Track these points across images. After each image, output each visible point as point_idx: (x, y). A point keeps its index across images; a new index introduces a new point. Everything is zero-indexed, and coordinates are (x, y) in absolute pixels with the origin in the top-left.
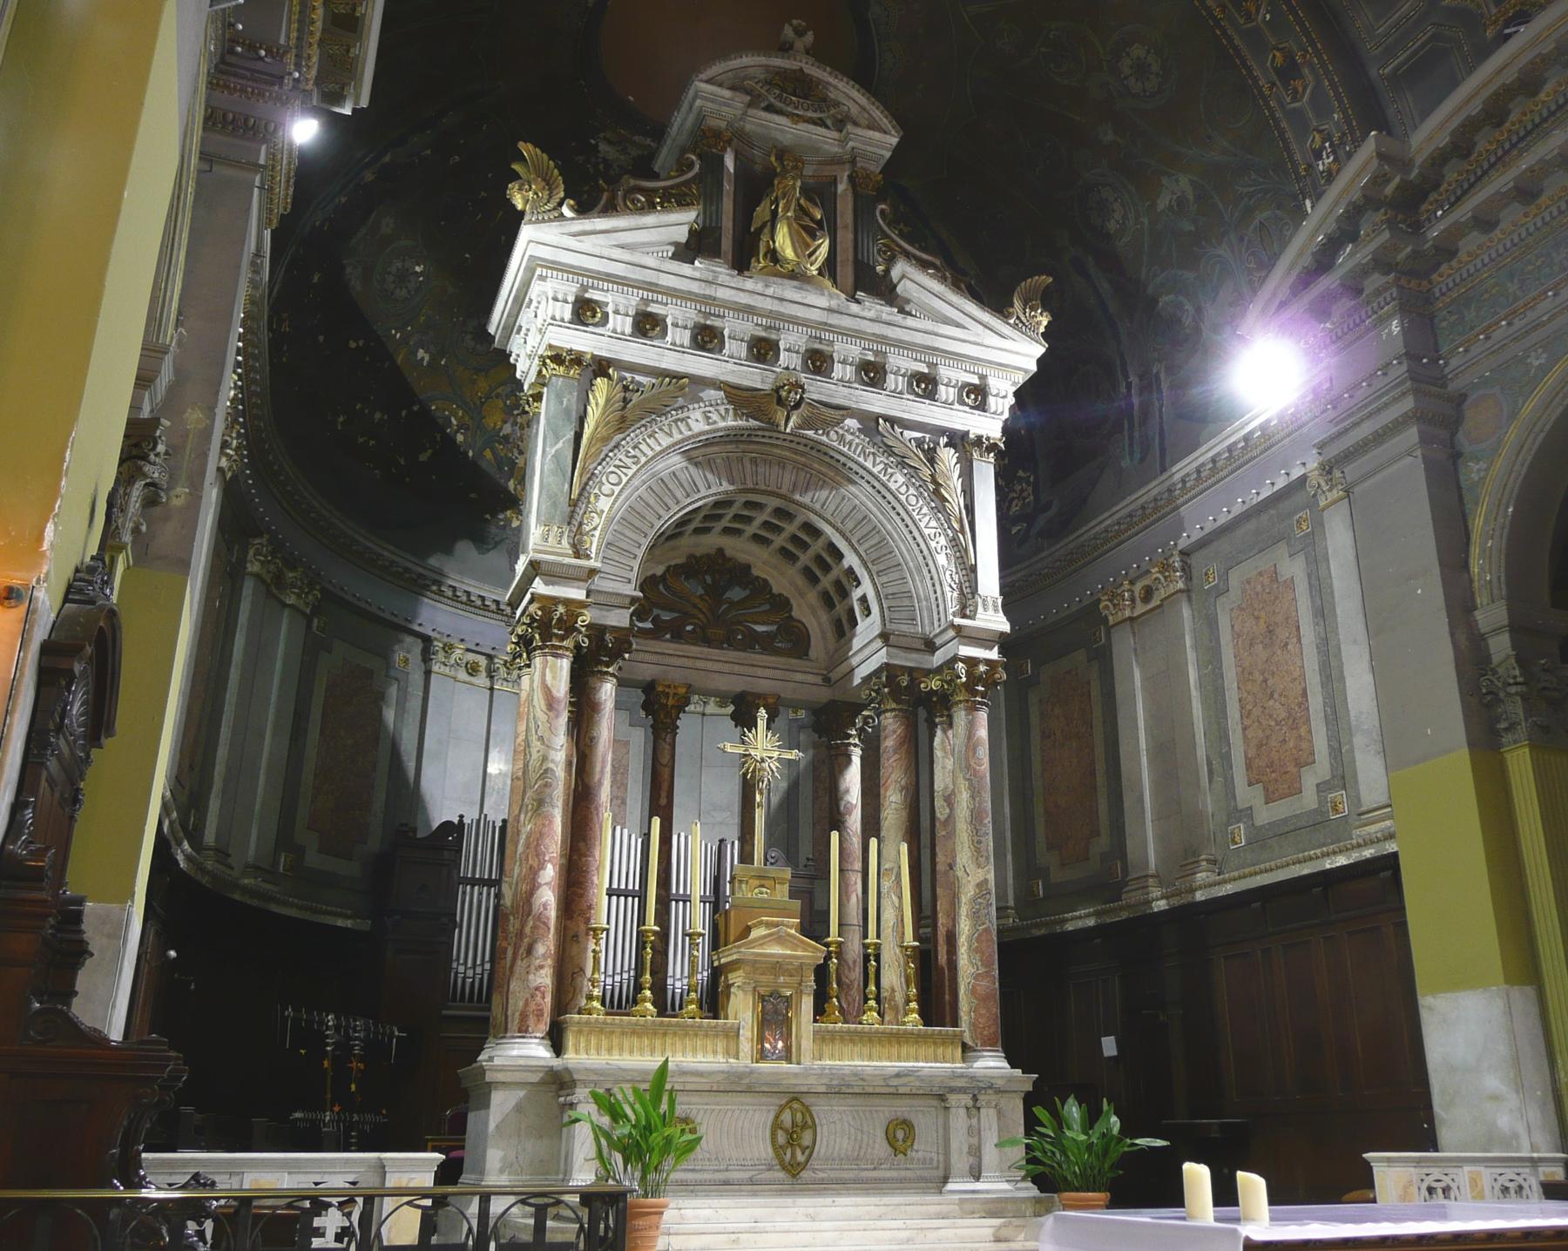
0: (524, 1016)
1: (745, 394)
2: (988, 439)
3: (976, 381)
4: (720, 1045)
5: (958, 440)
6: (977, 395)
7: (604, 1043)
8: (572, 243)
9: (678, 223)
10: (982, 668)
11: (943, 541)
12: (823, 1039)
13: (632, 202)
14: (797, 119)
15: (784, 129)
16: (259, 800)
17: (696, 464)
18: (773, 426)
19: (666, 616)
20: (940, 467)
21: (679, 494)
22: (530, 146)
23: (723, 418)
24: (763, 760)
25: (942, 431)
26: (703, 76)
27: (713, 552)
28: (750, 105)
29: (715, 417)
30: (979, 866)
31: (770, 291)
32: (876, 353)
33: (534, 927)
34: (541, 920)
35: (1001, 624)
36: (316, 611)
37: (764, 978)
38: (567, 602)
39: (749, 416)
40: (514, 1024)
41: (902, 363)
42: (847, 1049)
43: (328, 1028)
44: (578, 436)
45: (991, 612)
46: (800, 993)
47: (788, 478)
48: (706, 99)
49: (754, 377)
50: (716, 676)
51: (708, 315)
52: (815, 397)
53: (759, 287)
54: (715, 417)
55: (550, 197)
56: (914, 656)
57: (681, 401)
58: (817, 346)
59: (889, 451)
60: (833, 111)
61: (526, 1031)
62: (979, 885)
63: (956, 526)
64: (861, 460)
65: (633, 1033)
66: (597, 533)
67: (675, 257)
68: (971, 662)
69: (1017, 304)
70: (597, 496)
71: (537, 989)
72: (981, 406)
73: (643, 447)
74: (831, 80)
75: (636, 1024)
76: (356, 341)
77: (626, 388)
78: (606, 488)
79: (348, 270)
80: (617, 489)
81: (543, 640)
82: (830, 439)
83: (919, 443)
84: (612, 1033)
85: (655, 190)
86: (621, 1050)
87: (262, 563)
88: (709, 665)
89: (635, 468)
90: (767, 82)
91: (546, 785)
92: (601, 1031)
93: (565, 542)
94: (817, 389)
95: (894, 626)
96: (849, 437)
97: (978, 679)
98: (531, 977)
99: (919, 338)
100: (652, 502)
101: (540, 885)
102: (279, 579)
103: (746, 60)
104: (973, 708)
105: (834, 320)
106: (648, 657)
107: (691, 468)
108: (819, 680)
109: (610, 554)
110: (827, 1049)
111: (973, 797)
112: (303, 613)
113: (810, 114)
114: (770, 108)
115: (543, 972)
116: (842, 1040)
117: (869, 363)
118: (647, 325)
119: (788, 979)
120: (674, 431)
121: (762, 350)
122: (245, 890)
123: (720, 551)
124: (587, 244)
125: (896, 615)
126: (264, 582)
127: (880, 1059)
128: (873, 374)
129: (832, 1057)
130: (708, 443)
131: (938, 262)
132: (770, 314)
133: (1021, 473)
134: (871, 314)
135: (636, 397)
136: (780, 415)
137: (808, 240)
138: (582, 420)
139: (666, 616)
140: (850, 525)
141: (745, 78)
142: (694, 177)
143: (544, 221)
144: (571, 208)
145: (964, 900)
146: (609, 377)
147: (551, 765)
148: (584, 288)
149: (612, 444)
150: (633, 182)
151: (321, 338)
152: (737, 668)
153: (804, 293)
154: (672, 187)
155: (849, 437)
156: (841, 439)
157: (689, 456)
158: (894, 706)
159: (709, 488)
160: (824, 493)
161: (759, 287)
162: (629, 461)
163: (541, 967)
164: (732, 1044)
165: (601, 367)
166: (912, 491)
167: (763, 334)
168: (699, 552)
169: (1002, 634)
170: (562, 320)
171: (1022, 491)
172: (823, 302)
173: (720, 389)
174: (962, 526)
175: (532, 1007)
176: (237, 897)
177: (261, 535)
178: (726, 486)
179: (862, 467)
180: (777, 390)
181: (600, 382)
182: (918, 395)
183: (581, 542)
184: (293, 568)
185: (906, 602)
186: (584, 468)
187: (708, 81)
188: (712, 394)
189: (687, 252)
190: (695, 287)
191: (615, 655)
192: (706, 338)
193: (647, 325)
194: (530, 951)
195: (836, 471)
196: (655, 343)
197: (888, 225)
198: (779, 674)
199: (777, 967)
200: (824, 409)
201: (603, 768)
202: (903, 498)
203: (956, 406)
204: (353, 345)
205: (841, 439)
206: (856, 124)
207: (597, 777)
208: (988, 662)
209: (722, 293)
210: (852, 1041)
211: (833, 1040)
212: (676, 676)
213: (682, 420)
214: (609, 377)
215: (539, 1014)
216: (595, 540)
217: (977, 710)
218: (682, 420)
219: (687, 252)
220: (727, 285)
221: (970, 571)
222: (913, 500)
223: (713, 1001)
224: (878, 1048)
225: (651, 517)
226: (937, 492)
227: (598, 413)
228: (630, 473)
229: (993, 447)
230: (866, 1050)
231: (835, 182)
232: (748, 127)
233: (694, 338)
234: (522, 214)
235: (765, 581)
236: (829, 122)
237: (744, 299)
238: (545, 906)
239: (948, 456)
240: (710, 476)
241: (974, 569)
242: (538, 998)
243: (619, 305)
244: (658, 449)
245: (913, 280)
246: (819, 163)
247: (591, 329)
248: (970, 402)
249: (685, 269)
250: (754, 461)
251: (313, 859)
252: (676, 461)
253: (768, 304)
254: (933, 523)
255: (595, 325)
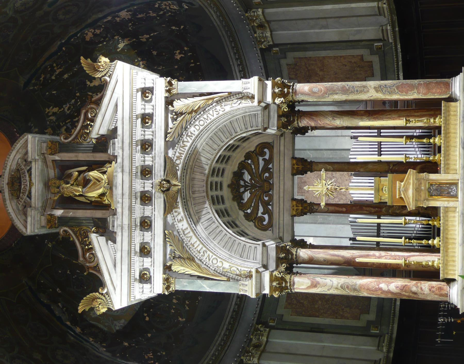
0: (441, 295)
1: (167, 205)
2: (166, 87)
3: (139, 94)
4: (451, 214)
5: (169, 102)
6: (146, 92)
7: (450, 268)
8: (118, 289)
9: (97, 241)
10: (277, 90)
11: (218, 108)
12: (448, 169)
13: (91, 258)
14: (31, 184)
15: (37, 189)
16: (351, 346)
17: (200, 219)
18: (178, 191)
19: (261, 210)
20: (184, 110)
21: (214, 226)
22: (79, 308)
23: (179, 213)
24: (327, 189)
25: (166, 109)
26: (24, 230)
27: (230, 190)
28: (31, 207)
29: (179, 217)
30: (368, 91)
31: (120, 200)
32: (137, 145)
33: (406, 292)
34: (404, 288)
35: (255, 80)
36: (266, 325)
37: (423, 196)
38: (271, 281)
39: (176, 202)
40: (444, 299)
41: (139, 133)
42: (452, 157)
43: (444, 321)
44: (199, 277)
45: (248, 85)
46: (428, 180)
47: (198, 176)
48: (34, 228)
49: (159, 201)
50: (285, 187)
51: (136, 225)
52: (162, 173)
53: (119, 205)
54: (179, 217)
55: (99, 298)
56: (272, 114)
57: (175, 233)
58: (139, 174)
59: (181, 135)
60: (23, 167)
61: (447, 294)
62: (377, 91)
63: (210, 102)
64: (187, 148)
65: (447, 251)
66: (239, 268)
67: (114, 242)
68: (274, 95)
69: (98, 75)
70: (223, 268)
71: (430, 290)
72: (151, 90)
73: (199, 249)
74: (8, 169)
75: (443, 251)
76: (145, 317)
77: (174, 257)
78: (219, 264)
79: (117, 328)
80: (219, 260)
81: (288, 289)
82: (180, 163)
83: (174, 120)
84: (447, 260)
85: (83, 249)
86: (454, 256)
87: (253, 357)
88: (282, 190)
89: (208, 252)
90: (18, 197)
91: (348, 287)
92: (446, 265)
93: (246, 283)
94: (159, 173)
95: (260, 125)
96: (177, 154)
97: (283, 91)
98: (425, 293)
99: (127, 127)
100: (220, 238)
101: (389, 290)
102: (257, 346)
103: (10, 210)
104: (295, 92)
105: (127, 169)
106: (281, 218)
107: (202, 220)
108: (282, 138)
109: (245, 256)
110: (452, 167)
111: (337, 94)
112: (269, 331)
113: (28, 178)
114: (29, 196)
115: (423, 288)
116: (448, 160)
117: (141, 147)
118: (145, 251)
119: (423, 185)
120: (189, 235)
121: (146, 198)
122: (388, 352)
123: (229, 186)
124: (117, 282)
125: (254, 124)
126: (260, 355)
127: (456, 142)
128: (146, 146)
129: (455, 165)
130: (190, 216)
131: (84, 111)
132: (130, 199)
133: (157, 6)
134: (120, 151)
135: (178, 253)
136: (174, 189)
137: (92, 183)
138: (191, 276)
139: (261, 210)
140: (215, 146)
141: (18, 209)
142: (71, 230)
143: (111, 301)
144: (103, 289)
145: (384, 97)
146: (171, 265)
147: (339, 285)
148: (135, 279)
149: (199, 262)
150: (81, 259)
151: (149, 335)
152: (282, 178)
153: (118, 185)
154: (79, 240)
155: (177, 154)
156: (179, 158)
157: (196, 223)
158: (296, 122)
159: (208, 212)
160: (203, 159)
161: (119, 205)
162: (206, 255)
163: (421, 288)
164: (451, 209)
165: (167, 268)
166: (197, 123)
167: (139, 199)
168: (231, 196)
169: (260, 80)
170: (151, 288)
171: (165, 5)
172: (120, 175)
173: (167, 217)
174: (210, 99)
175: (437, 292)
176: (391, 355)
177: (242, 360)
178: (207, 205)
179: (190, 148)
180: (163, 192)
181: (173, 268)
182: (152, 122)
183: (245, 275)
184: (251, 340)
185: (247, 118)
186: (212, 275)
187: (26, 227)
188: (169, 218)
189: (111, 237)
190: (126, 234)
191: (288, 252)
192: (146, 224)
193: (145, 251)
194: (415, 293)
195: (193, 157)
196: (152, 246)
197: (71, 135)
198: (282, 158)
199: (417, 190)
200: (167, 167)
201: (336, 255)
202: (202, 128)
203: (153, 103)
204: (147, 319)
205: (179, 158)
206: (27, 153)
207: (340, 258)
208: (273, 87)
209: (126, 222)
210: (448, 155)
211: (448, 164)
212: (288, 204)
213: (184, 232)
214: (171, 265)
215: (440, 289)
216: (242, 269)
217: (296, 91)
218: (184, 232)
219: (111, 237)
220: (121, 221)
221: (231, 95)
222: (202, 123)
223: (432, 213)
224: (451, 156)
225: (226, 239)
226: (196, 111)
227: (187, 270)
228: (211, 254)
229: (170, 83)
230: (452, 149)
231: (54, 161)
232: (40, 205)
233: (147, 230)
234: (109, 308)
235: (239, 164)
236: (28, 168)
237: (126, 212)
238: (397, 287)
239: (178, 105)
240: (204, 212)
241: (230, 93)
242: (434, 289)
243: (139, 263)
244: (198, 242)
245: (100, 128)
246: (47, 167)
247: (152, 274)
248: (150, 96)
249: (119, 239)
250: (194, 192)
251: (372, 316)
252: (200, 228)
253: (126, 201)
254: (211, 112)
255: (150, 273)
